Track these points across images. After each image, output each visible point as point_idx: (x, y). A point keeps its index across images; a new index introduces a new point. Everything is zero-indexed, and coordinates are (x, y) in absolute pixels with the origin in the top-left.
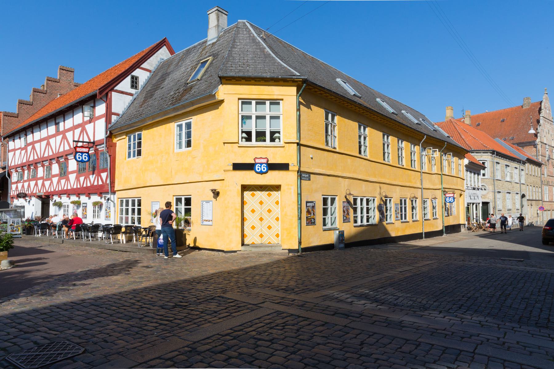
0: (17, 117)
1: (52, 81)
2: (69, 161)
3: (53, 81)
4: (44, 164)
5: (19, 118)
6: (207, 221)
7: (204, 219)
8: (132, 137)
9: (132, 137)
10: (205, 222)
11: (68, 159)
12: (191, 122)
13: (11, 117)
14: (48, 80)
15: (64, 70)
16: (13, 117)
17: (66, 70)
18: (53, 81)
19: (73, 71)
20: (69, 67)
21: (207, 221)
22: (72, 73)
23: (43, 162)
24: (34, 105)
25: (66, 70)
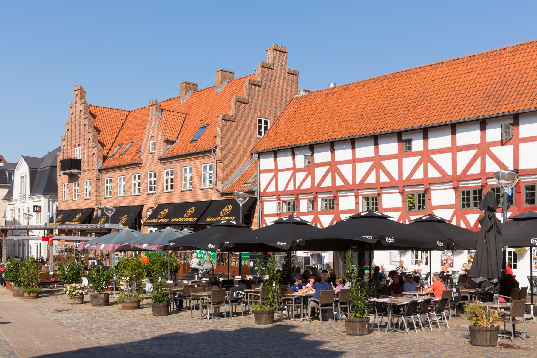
0: (234, 122)
1: (266, 67)
2: (432, 191)
3: (268, 68)
4: (358, 193)
5: (236, 122)
6: (395, 262)
7: (392, 260)
8: (77, 184)
9: (77, 184)
10: (392, 262)
11: (430, 189)
12: (212, 165)
13: (229, 121)
14: (250, 84)
15: (278, 50)
16: (231, 121)
17: (279, 51)
18: (268, 68)
19: (286, 51)
20: (282, 45)
21: (395, 262)
22: (285, 55)
23: (357, 190)
24: (249, 103)
25: (279, 51)
